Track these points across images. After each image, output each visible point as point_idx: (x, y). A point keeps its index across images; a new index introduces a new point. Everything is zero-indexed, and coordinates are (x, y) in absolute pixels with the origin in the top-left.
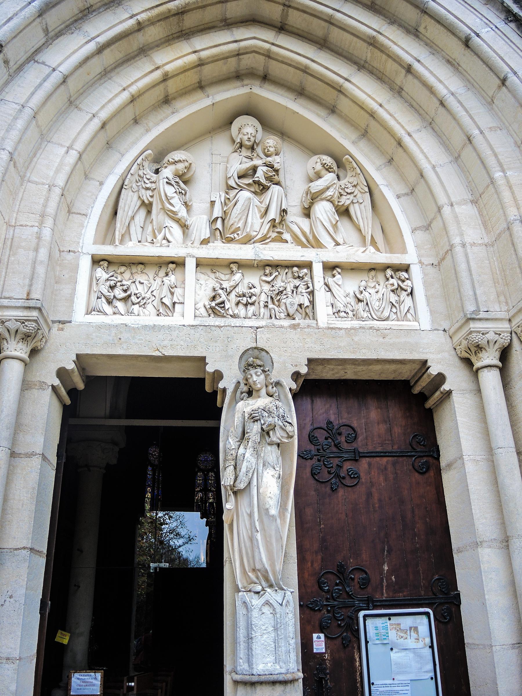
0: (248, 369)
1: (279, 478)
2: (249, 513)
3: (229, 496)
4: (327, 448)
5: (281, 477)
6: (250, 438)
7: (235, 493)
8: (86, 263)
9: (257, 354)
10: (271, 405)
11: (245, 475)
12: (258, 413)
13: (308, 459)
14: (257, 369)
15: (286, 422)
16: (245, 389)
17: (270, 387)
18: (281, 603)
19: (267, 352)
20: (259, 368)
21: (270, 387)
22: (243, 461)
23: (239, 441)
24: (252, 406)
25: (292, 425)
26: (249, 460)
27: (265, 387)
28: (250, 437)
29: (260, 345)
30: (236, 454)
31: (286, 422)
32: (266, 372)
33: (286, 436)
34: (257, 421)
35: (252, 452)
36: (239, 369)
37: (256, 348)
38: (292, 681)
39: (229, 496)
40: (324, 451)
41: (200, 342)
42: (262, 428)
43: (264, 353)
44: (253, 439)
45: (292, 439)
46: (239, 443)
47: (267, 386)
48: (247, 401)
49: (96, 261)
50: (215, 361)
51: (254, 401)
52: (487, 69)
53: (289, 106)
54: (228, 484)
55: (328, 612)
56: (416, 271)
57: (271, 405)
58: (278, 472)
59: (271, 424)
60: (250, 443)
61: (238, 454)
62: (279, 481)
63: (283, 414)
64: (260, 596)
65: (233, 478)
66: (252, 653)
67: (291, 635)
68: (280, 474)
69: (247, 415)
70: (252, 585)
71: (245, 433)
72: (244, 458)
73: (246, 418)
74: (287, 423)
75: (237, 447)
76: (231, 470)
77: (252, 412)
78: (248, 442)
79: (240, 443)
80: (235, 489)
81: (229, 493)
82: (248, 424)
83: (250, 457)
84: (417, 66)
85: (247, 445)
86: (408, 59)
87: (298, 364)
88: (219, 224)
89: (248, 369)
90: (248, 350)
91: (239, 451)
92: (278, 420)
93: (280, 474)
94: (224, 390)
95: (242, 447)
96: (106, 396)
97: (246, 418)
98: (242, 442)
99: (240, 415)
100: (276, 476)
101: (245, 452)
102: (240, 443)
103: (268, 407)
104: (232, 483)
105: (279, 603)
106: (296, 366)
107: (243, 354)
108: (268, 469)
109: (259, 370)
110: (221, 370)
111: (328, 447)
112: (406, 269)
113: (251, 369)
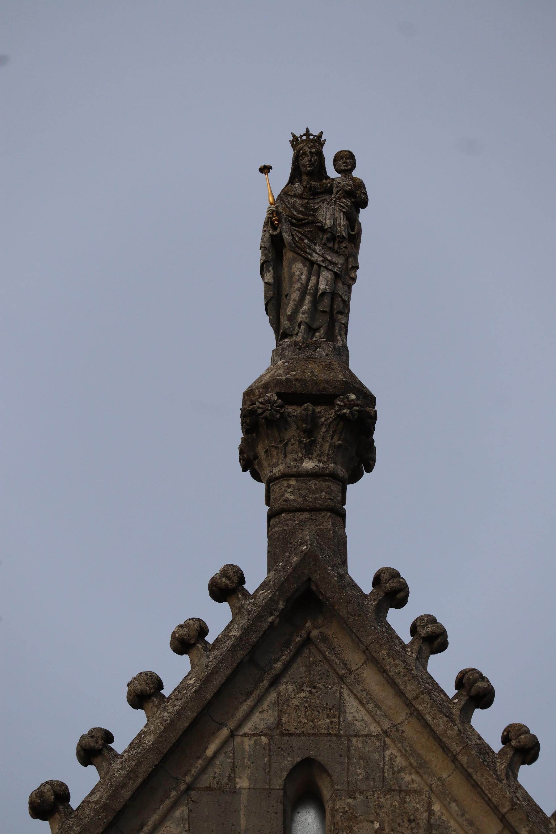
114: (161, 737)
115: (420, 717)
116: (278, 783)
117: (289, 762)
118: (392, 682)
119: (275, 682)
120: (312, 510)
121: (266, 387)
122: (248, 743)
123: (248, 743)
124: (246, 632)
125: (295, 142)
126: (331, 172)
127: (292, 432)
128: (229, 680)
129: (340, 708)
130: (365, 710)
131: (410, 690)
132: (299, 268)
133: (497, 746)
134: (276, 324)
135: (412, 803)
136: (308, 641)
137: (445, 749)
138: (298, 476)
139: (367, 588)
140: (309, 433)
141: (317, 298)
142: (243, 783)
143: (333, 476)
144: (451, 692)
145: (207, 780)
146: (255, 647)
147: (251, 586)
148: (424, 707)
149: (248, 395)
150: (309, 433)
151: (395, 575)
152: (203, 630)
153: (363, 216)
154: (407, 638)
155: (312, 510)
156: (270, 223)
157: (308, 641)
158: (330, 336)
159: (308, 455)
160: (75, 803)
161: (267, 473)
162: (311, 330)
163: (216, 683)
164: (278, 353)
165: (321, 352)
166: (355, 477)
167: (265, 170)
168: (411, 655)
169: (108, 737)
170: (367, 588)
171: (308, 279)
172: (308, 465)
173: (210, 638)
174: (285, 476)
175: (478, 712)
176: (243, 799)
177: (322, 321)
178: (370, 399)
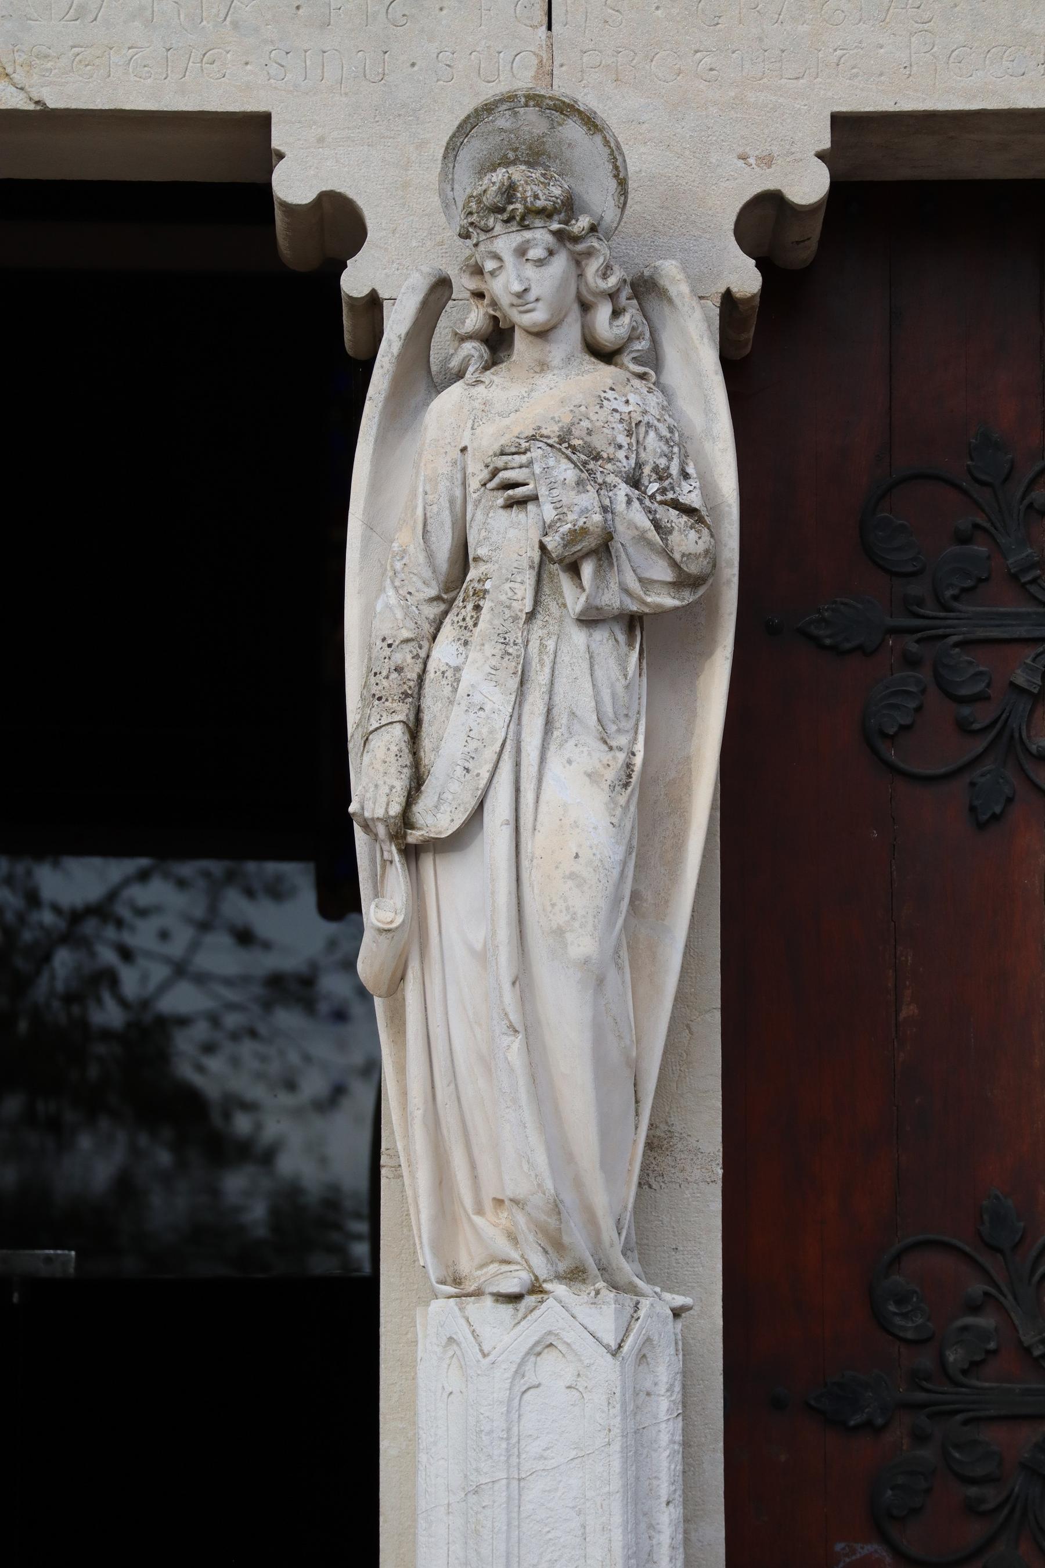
0: (487, 230)
1: (626, 785)
2: (479, 946)
3: (384, 867)
4: (964, 590)
5: (634, 779)
6: (486, 592)
7: (412, 854)
9: (537, 131)
10: (604, 414)
11: (459, 771)
12: (529, 464)
13: (850, 651)
14: (527, 228)
15: (676, 505)
16: (475, 318)
17: (603, 313)
18: (614, 1345)
19: (591, 123)
20: (538, 223)
21: (603, 313)
22: (451, 702)
23: (438, 598)
24: (506, 421)
25: (701, 520)
26: (477, 698)
27: (575, 310)
28: (488, 585)
29: (563, 88)
30: (418, 669)
31: (676, 505)
32: (576, 239)
33: (668, 575)
34: (521, 503)
35: (494, 662)
36: (446, 206)
37: (533, 99)
38: (543, 1282)
39: (384, 867)
40: (946, 609)
41: (235, 25)
42: (542, 547)
43: (572, 130)
44: (503, 598)
45: (701, 591)
46: (433, 611)
47: (585, 307)
48: (481, 388)
50: (321, 140)
51: (517, 390)
52: (557, 672)
53: (396, 1134)
54: (380, 813)
55: (920, 1438)
57: (604, 414)
58: (621, 756)
59: (584, 531)
60: (485, 613)
61: (431, 666)
62: (622, 800)
63: (662, 462)
64: (520, 1315)
65: (400, 784)
66: (478, 1553)
67: (664, 1489)
68: (629, 766)
69: (477, 473)
70: (493, 1268)
71: (471, 557)
72: (455, 690)
73: (474, 484)
74: (673, 513)
75: (427, 629)
76: (394, 749)
77: (500, 462)
78: (477, 608)
79: (443, 607)
80: (414, 837)
81: (386, 856)
82: (480, 516)
83: (487, 688)
85: (470, 623)
87: (776, 150)
89: (487, 230)
90: (488, 108)
91: (435, 654)
92: (629, 502)
93: (629, 766)
94: (373, 303)
95: (448, 630)
96: (1010, 1317)
97: (474, 484)
98: (451, 603)
99: (443, 466)
100: (610, 775)
101: (461, 659)
102: (443, 607)
103: (585, 424)
104: (395, 809)
105: (607, 1347)
106: (767, 161)
107: (465, 128)
108: (571, 743)
109: (540, 237)
110: (351, 194)
111: (969, 583)
113: (499, 228)
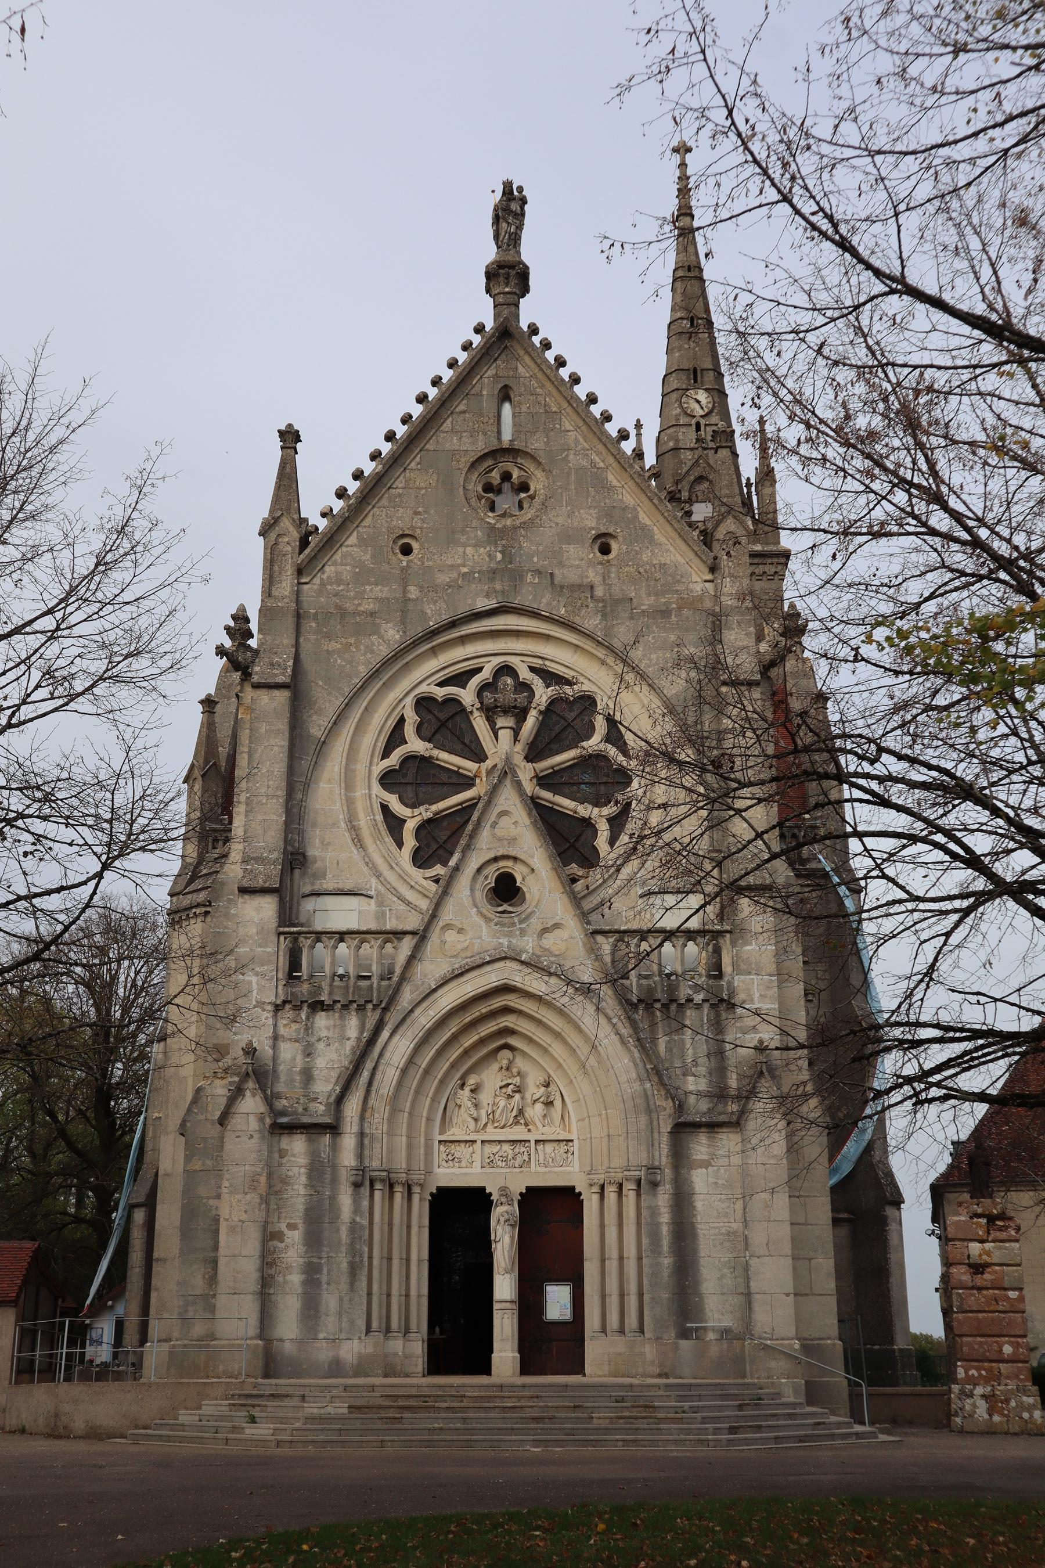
8: (436, 1143)
49: (440, 1142)
56: (576, 1142)
84: (577, 1050)
86: (575, 1047)
88: (491, 1116)
112: (572, 1141)
114: (457, 377)
115: (542, 370)
116: (496, 393)
117: (500, 386)
118: (533, 359)
119: (495, 360)
120: (508, 304)
121: (493, 263)
122: (486, 380)
123: (486, 380)
124: (485, 343)
125: (504, 183)
126: (516, 193)
127: (501, 279)
128: (479, 359)
129: (516, 368)
130: (281, 810)
131: (539, 361)
132: (504, 225)
133: (567, 379)
134: (497, 244)
135: (540, 398)
136: (506, 347)
137: (550, 380)
138: (503, 293)
139: (526, 329)
140: (507, 278)
141: (510, 235)
142: (485, 393)
143: (515, 293)
144: (552, 362)
145: (473, 392)
146: (488, 349)
147: (487, 329)
148: (543, 367)
149: (487, 266)
150: (507, 278)
151: (534, 324)
152: (471, 344)
153: (526, 207)
154: (538, 345)
155: (508, 304)
156: (495, 210)
157: (506, 347)
158: (515, 247)
159: (507, 286)
160: (430, 399)
161: (493, 293)
162: (508, 245)
163: (476, 360)
164: (497, 253)
165: (512, 252)
166: (523, 296)
167: (493, 191)
168: (540, 350)
169: (441, 378)
170: (526, 329)
171: (73, 978)
172: (507, 290)
173: (474, 346)
174: (499, 293)
175: (561, 369)
176: (485, 398)
177: (513, 242)
178: (528, 268)
